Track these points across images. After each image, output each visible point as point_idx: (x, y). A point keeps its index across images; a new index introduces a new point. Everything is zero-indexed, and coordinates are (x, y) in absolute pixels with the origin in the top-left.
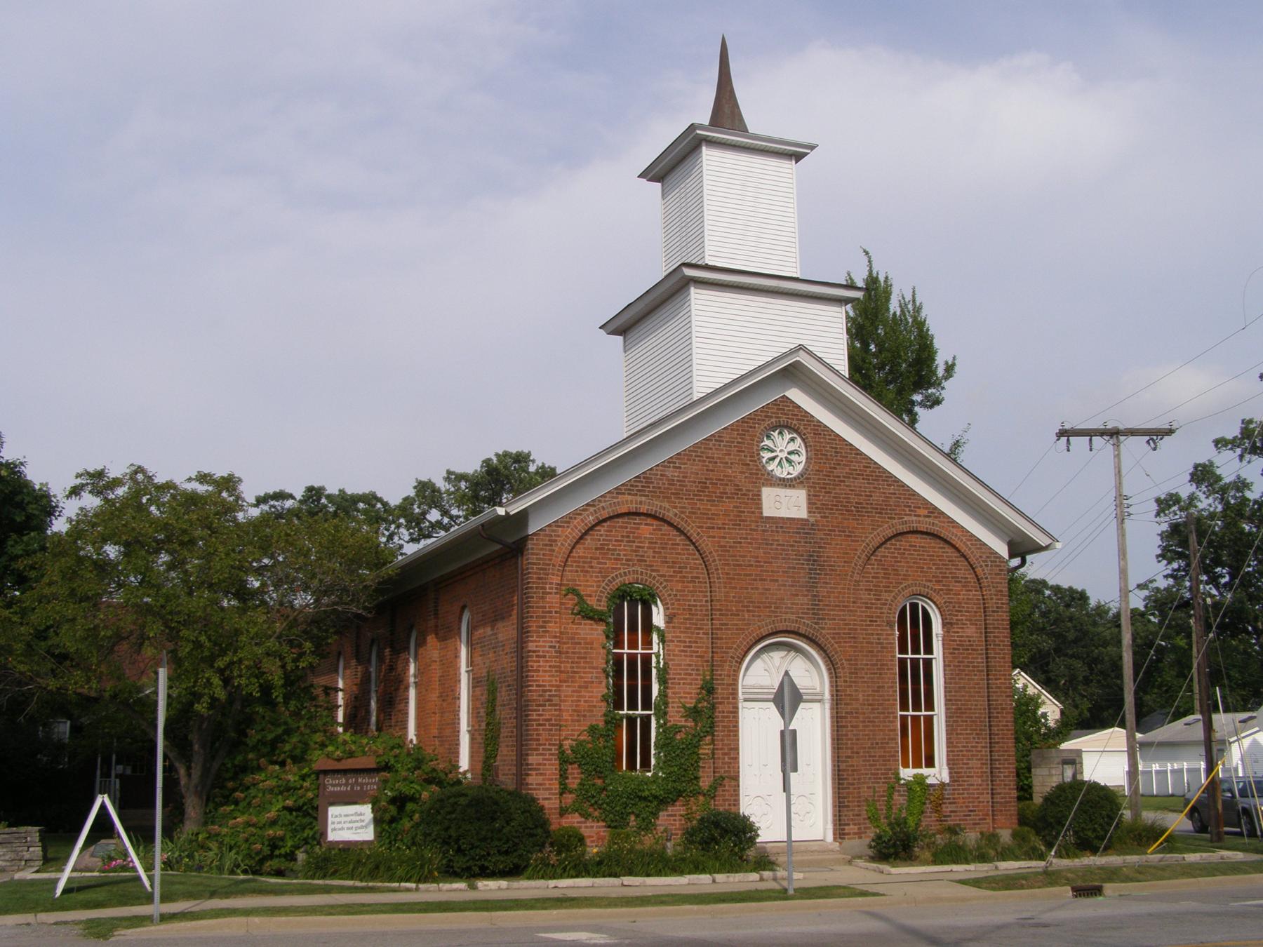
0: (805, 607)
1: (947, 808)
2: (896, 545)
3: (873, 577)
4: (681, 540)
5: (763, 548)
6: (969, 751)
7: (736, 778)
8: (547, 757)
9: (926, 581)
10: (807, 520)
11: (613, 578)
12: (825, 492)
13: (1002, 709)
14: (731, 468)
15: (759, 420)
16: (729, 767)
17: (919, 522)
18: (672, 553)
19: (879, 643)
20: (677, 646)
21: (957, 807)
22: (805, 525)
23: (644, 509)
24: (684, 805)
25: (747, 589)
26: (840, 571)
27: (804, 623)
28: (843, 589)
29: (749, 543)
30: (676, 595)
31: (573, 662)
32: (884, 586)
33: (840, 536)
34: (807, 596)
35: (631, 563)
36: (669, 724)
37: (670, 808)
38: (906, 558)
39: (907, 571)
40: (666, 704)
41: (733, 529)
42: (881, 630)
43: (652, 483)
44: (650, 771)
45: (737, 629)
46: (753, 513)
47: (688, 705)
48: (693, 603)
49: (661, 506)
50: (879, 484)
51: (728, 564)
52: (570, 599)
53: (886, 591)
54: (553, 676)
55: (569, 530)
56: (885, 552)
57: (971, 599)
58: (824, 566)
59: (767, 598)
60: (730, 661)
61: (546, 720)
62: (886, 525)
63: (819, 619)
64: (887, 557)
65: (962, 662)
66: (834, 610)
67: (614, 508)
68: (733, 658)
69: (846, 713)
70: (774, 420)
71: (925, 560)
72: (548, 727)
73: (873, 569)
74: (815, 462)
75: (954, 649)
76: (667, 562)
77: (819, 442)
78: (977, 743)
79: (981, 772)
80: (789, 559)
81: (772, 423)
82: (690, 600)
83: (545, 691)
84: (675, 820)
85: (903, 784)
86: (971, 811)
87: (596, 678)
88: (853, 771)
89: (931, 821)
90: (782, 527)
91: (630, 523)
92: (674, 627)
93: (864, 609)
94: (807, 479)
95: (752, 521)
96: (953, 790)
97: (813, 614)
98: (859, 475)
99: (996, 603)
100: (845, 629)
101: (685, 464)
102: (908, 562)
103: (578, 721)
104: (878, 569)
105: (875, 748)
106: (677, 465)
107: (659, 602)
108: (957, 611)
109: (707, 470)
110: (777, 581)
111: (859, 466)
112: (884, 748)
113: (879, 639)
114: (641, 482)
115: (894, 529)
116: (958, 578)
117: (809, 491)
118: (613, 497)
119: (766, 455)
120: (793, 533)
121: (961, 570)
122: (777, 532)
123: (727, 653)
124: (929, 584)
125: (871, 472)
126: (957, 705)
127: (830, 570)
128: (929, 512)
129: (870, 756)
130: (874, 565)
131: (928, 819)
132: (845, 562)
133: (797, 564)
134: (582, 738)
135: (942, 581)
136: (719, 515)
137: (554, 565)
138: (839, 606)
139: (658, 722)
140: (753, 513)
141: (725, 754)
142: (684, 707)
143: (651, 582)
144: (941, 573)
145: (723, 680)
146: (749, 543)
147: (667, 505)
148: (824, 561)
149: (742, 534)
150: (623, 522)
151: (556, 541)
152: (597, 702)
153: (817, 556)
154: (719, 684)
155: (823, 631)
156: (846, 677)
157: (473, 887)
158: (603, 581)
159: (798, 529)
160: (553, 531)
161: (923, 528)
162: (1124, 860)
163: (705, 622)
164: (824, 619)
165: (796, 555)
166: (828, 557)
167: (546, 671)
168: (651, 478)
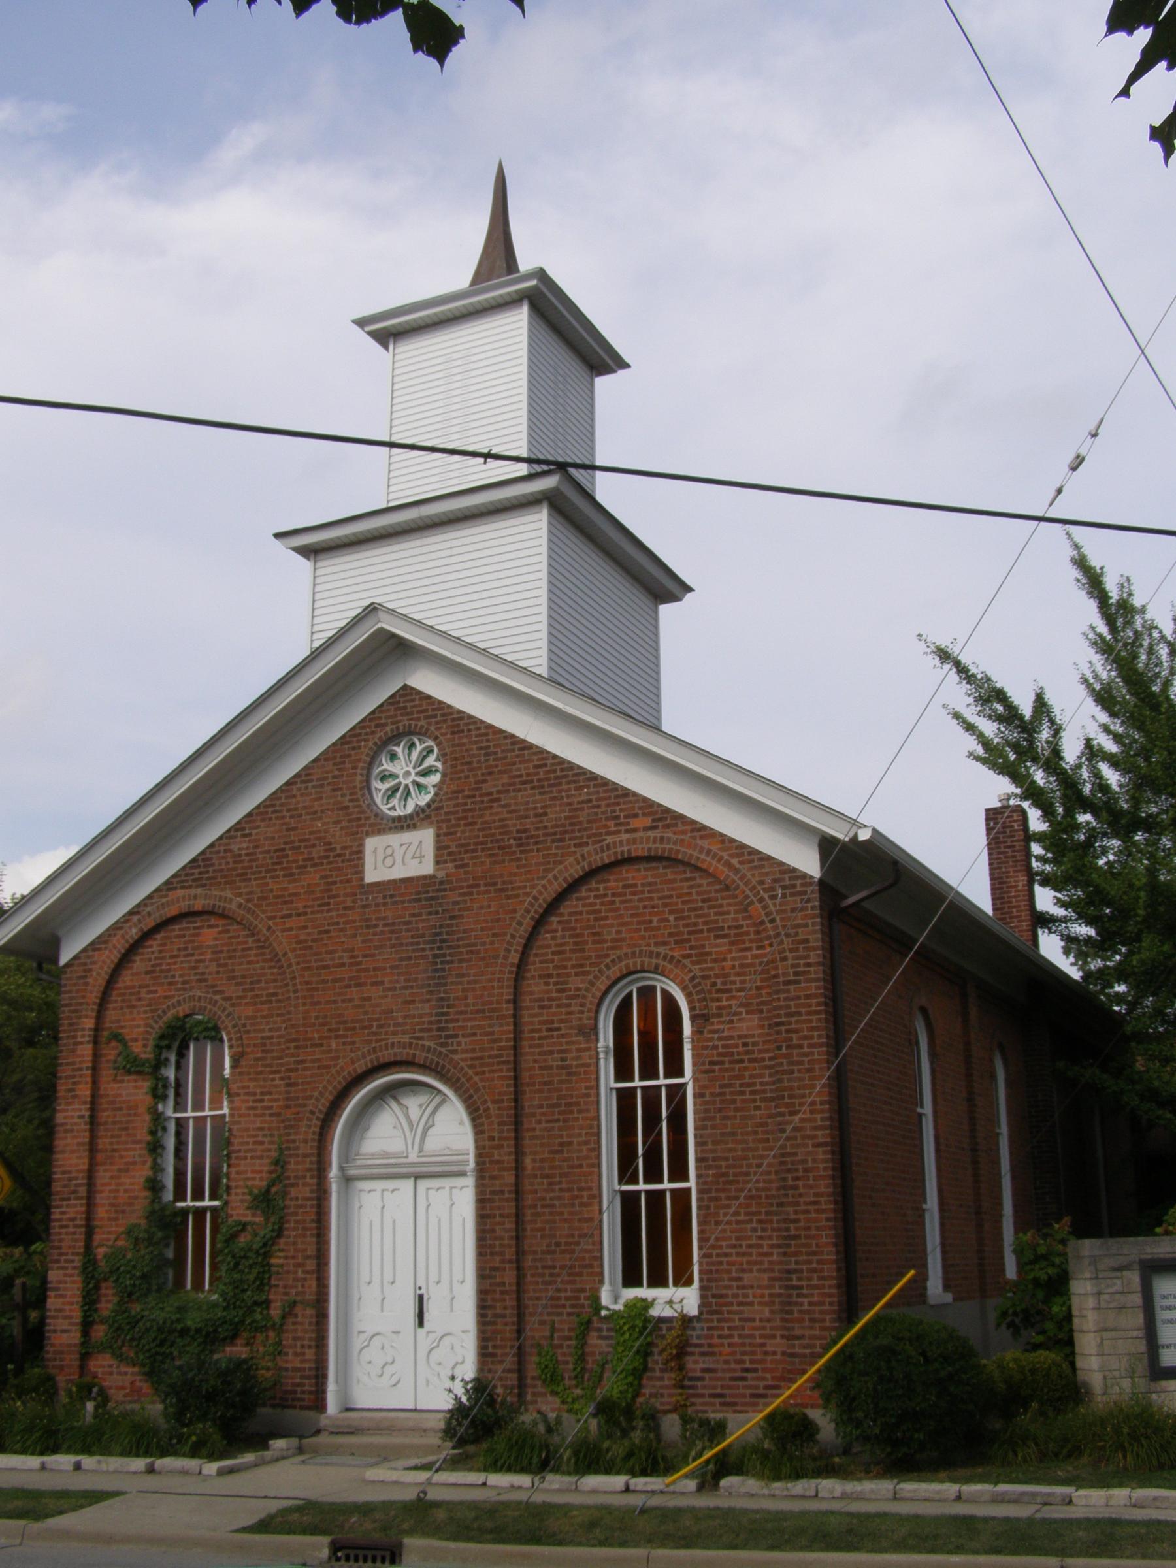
1: (695, 1364)
2: (597, 889)
3: (554, 953)
6: (744, 1254)
9: (656, 944)
12: (465, 825)
13: (806, 1170)
15: (366, 734)
16: (303, 1286)
17: (635, 841)
18: (241, 964)
19: (563, 1067)
22: (428, 885)
25: (335, 1002)
26: (486, 951)
27: (423, 1046)
28: (490, 980)
29: (341, 930)
30: (244, 1025)
31: (112, 1137)
32: (573, 966)
34: (428, 1001)
38: (618, 909)
41: (318, 912)
42: (567, 1043)
46: (348, 881)
50: (560, 791)
51: (309, 968)
52: (114, 1048)
53: (577, 974)
56: (576, 906)
57: (748, 965)
58: (459, 946)
59: (366, 1013)
60: (310, 1120)
63: (448, 1037)
64: (581, 913)
65: (729, 1086)
66: (475, 1019)
68: (312, 1113)
70: (388, 729)
73: (553, 938)
74: (451, 779)
75: (712, 1063)
76: (233, 978)
77: (458, 745)
78: (760, 1238)
79: (771, 1295)
80: (401, 944)
82: (263, 1031)
83: (70, 1179)
85: (606, 1318)
86: (747, 1370)
88: (502, 1293)
89: (662, 1387)
91: (188, 928)
92: (241, 1073)
93: (536, 1011)
95: (347, 895)
96: (709, 1329)
97: (439, 1029)
98: (525, 783)
99: (793, 966)
100: (492, 1048)
102: (621, 916)
103: (116, 1219)
104: (563, 937)
105: (554, 1252)
108: (718, 991)
110: (382, 983)
113: (562, 1059)
115: (585, 864)
116: (722, 928)
117: (439, 828)
118: (162, 897)
120: (410, 901)
121: (728, 913)
122: (385, 904)
123: (305, 1105)
127: (468, 953)
129: (544, 1267)
130: (556, 931)
131: (658, 1383)
132: (494, 935)
133: (413, 951)
134: (120, 1243)
135: (689, 940)
138: (483, 1011)
140: (348, 881)
141: (299, 1265)
145: (297, 1148)
146: (341, 930)
147: (228, 894)
150: (180, 929)
151: (90, 970)
153: (447, 933)
154: (290, 1156)
155: (456, 1057)
160: (89, 957)
161: (640, 850)
162: (1109, 1498)
164: (456, 1036)
165: (412, 937)
166: (465, 931)
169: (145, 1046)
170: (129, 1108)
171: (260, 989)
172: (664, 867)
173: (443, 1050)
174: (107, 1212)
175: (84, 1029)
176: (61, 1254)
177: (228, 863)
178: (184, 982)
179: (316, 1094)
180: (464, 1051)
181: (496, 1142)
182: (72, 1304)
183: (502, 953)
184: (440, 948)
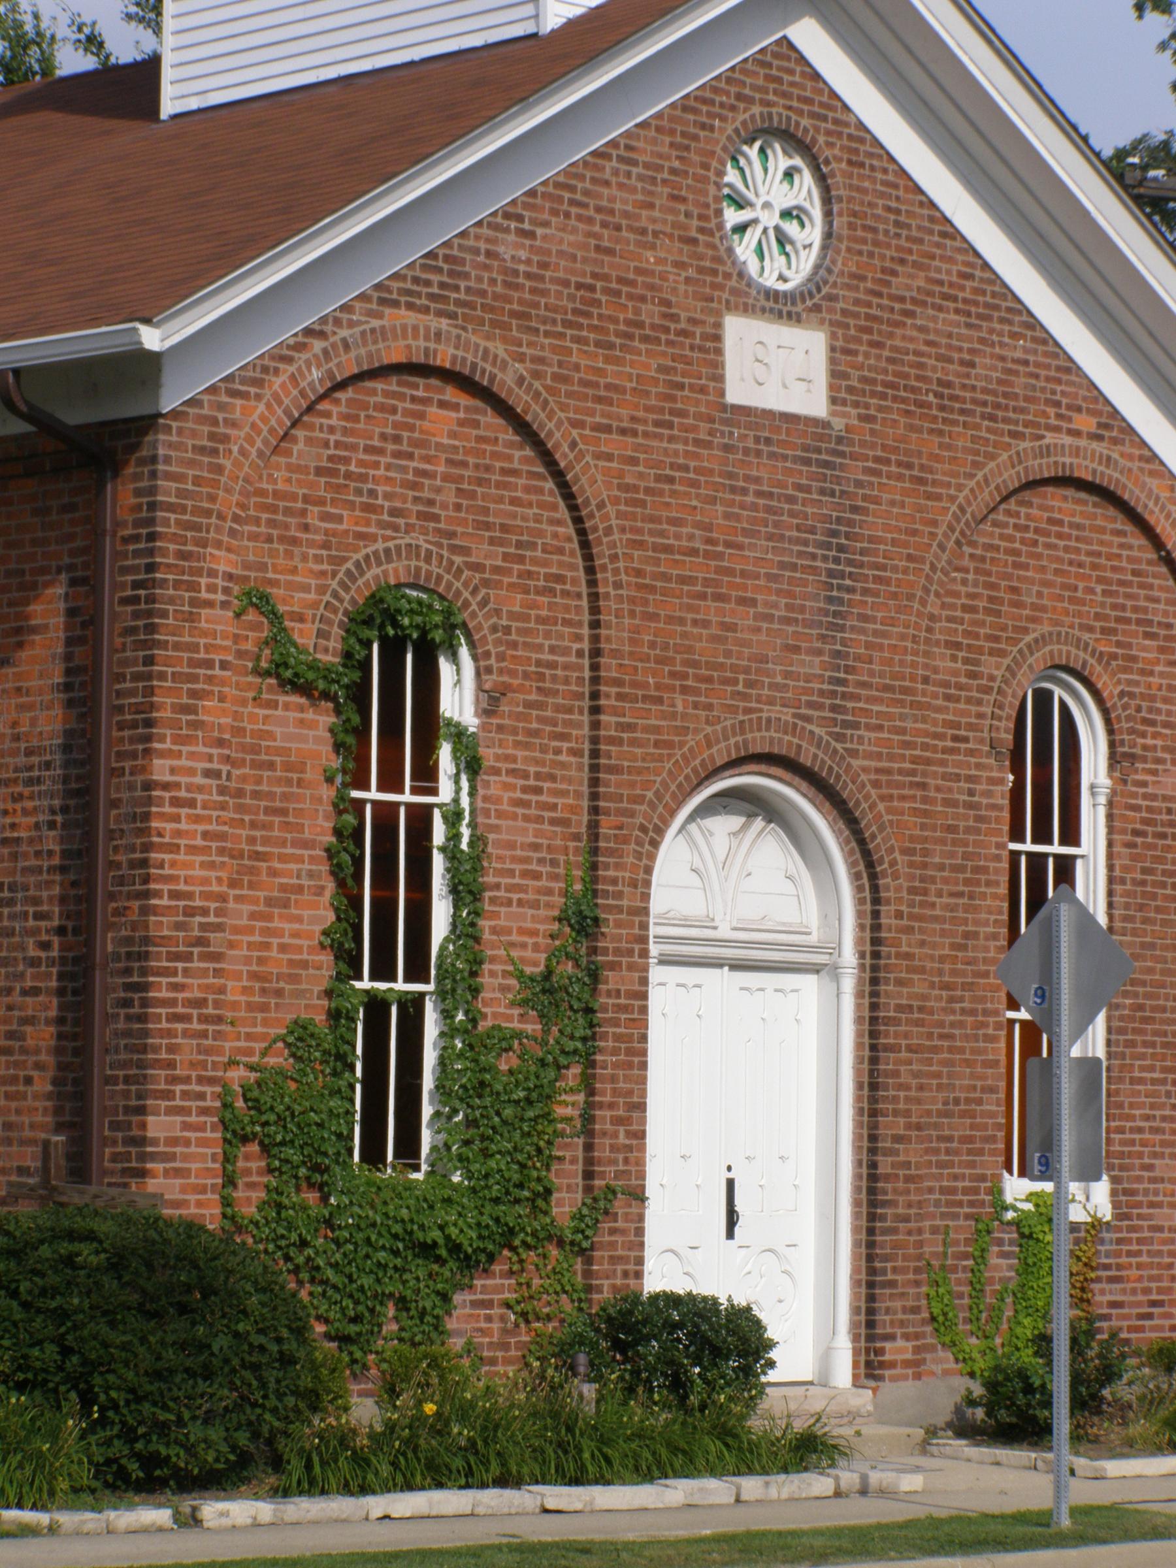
0: (816, 686)
4: (525, 460)
5: (724, 502)
7: (639, 1196)
8: (193, 1119)
10: (826, 425)
11: (358, 564)
14: (653, 247)
15: (722, 105)
16: (626, 1161)
18: (500, 500)
20: (507, 787)
21: (1124, 1291)
22: (821, 438)
23: (444, 356)
24: (511, 1273)
27: (812, 732)
31: (253, 825)
33: (900, 477)
34: (819, 652)
35: (401, 521)
36: (483, 1026)
37: (478, 1283)
39: (1040, 595)
40: (476, 962)
43: (466, 276)
44: (417, 1168)
45: (657, 744)
47: (528, 970)
48: (547, 657)
49: (486, 351)
51: (640, 545)
54: (211, 866)
55: (261, 407)
58: (861, 565)
59: (728, 654)
61: (191, 1003)
62: (1005, 456)
67: (373, 348)
69: (899, 1008)
70: (756, 110)
71: (1080, 565)
72: (196, 1026)
73: (964, 582)
74: (849, 250)
75: (1136, 833)
76: (488, 526)
80: (782, 538)
81: (753, 117)
82: (539, 648)
83: (190, 912)
84: (489, 1319)
85: (1009, 1223)
86: (1153, 1304)
87: (311, 875)
90: (768, 441)
91: (401, 397)
92: (500, 728)
94: (831, 298)
97: (834, 708)
98: (946, 297)
101: (546, 224)
103: (264, 1008)
106: (526, 226)
107: (464, 652)
109: (598, 248)
111: (949, 272)
112: (972, 1115)
113: (971, 793)
114: (439, 270)
115: (1020, 468)
116: (1150, 623)
117: (833, 336)
118: (371, 314)
119: (732, 217)
120: (795, 459)
121: (1156, 600)
122: (758, 453)
124: (1086, 636)
125: (976, 291)
126: (1136, 995)
128: (1099, 425)
130: (967, 571)
132: (910, 558)
133: (800, 554)
134: (272, 1061)
136: (623, 391)
137: (221, 517)
139: (447, 1015)
142: (520, 976)
143: (449, 585)
144: (1114, 607)
145: (619, 895)
147: (499, 349)
148: (863, 552)
149: (676, 453)
150: (386, 394)
151: (226, 439)
152: (311, 950)
153: (847, 536)
155: (856, 763)
156: (899, 900)
157: (193, 1521)
158: (334, 574)
159: (806, 448)
163: (575, 717)
167: (192, 850)
168: (462, 262)
169: (321, 634)
170: (288, 767)
171: (535, 561)
172: (1095, 505)
173: (839, 746)
174: (246, 990)
175: (212, 573)
176: (174, 1080)
177: (493, 281)
178: (394, 512)
179: (650, 794)
180: (869, 756)
181: (905, 922)
182: (203, 1190)
183: (919, 593)
184: (837, 560)
